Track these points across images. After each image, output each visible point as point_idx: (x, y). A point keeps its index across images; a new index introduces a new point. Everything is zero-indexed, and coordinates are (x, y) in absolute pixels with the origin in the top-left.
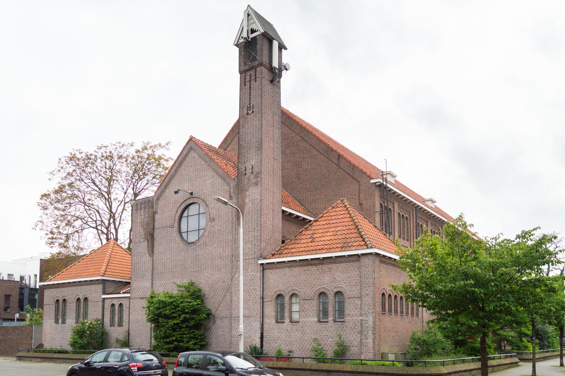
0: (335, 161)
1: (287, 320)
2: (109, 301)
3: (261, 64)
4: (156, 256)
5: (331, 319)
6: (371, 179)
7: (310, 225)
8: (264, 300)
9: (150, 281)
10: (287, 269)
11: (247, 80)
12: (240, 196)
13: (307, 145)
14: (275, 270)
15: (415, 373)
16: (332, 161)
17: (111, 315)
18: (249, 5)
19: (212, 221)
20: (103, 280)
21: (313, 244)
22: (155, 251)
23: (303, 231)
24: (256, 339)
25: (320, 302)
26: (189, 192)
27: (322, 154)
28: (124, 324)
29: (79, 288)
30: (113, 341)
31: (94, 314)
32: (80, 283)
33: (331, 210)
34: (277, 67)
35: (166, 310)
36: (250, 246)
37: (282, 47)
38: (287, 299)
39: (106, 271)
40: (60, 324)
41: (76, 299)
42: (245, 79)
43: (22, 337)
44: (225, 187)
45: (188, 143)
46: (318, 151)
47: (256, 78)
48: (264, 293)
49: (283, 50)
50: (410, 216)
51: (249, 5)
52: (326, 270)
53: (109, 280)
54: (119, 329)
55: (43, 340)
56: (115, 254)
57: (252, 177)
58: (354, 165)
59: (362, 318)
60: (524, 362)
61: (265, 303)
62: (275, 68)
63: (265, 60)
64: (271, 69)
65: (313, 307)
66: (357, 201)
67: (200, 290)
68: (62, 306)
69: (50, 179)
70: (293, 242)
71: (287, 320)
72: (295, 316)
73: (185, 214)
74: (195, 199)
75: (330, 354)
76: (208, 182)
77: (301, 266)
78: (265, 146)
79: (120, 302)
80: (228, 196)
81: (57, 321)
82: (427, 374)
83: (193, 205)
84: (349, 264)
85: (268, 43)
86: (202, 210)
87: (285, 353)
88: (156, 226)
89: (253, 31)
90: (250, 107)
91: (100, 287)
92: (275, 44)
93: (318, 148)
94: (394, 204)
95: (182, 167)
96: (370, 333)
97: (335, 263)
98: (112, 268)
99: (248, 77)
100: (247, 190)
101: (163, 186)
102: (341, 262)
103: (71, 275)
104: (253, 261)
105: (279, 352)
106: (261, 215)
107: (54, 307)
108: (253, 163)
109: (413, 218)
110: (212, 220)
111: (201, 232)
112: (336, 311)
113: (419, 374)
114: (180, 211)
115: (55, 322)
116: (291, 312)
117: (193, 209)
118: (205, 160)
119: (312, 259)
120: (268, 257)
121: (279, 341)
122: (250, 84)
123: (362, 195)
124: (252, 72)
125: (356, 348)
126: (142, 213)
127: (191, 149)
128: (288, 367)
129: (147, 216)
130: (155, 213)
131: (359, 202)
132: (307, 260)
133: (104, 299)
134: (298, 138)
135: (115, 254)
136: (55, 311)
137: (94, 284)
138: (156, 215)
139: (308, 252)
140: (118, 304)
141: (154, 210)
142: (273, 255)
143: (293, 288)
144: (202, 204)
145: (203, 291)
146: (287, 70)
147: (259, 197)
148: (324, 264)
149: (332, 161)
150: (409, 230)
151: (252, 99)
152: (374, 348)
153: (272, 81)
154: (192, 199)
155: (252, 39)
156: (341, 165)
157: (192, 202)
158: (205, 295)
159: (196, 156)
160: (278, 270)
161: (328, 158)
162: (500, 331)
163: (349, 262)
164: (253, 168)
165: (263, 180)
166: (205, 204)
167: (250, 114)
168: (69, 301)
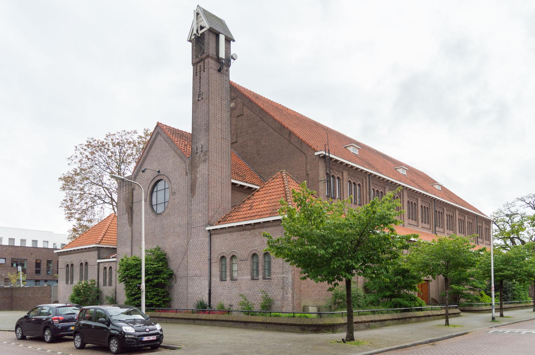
0: (287, 136)
1: (228, 278)
2: (103, 264)
3: (208, 56)
4: (134, 225)
5: (261, 276)
6: (315, 152)
7: (252, 195)
8: (212, 262)
9: (130, 247)
10: (228, 234)
11: (198, 71)
12: (193, 172)
13: (265, 125)
14: (219, 235)
15: (310, 323)
16: (284, 138)
17: (104, 277)
18: (198, 5)
19: (174, 194)
20: (97, 247)
21: (251, 211)
22: (134, 222)
23: (245, 200)
24: (205, 295)
25: (253, 262)
26: (157, 170)
27: (277, 132)
28: (113, 283)
29: (81, 254)
30: (104, 298)
31: (92, 275)
32: (82, 251)
33: (271, 181)
34: (224, 58)
35: (132, 271)
36: (201, 215)
37: (229, 40)
38: (228, 260)
39: (102, 239)
40: (69, 284)
41: (80, 264)
42: (196, 70)
43: (44, 296)
44: (183, 165)
45: (155, 129)
46: (273, 129)
47: (204, 68)
48: (212, 255)
49: (232, 42)
50: (363, 183)
51: (198, 5)
52: (257, 234)
53: (103, 247)
54: (110, 288)
55: (58, 298)
56: (113, 225)
57: (202, 154)
58: (302, 140)
59: (283, 275)
60: (473, 313)
61: (212, 264)
62: (221, 59)
63: (212, 51)
64: (218, 59)
65: (247, 266)
66: (304, 172)
67: (165, 255)
68: (71, 270)
69: (69, 164)
70: (236, 210)
71: (228, 278)
72: (235, 275)
73: (155, 190)
74: (161, 176)
75: (257, 307)
76: (171, 161)
77: (238, 231)
78: (213, 127)
79: (110, 266)
80: (185, 172)
81: (67, 283)
82: (321, 324)
83: (160, 182)
84: (274, 228)
85: (215, 37)
86: (167, 186)
87: (227, 307)
88: (134, 201)
89: (202, 28)
90: (200, 95)
91: (95, 253)
92: (222, 38)
93: (273, 126)
94: (343, 173)
95: (152, 149)
96: (290, 289)
97: (263, 227)
98: (109, 237)
99: (198, 68)
100: (197, 167)
101: (139, 166)
102: (268, 227)
103: (78, 244)
104: (202, 228)
105: (222, 307)
106: (208, 188)
107: (65, 271)
108: (202, 143)
109: (366, 185)
110: (173, 193)
111: (166, 204)
112: (265, 269)
113: (313, 324)
114: (151, 187)
115: (66, 283)
116: (232, 271)
117: (161, 185)
118: (168, 142)
119: (246, 225)
120: (215, 224)
121: (222, 297)
122: (200, 74)
123: (308, 166)
124: (202, 64)
125: (280, 302)
126: (124, 190)
127: (158, 133)
128: (216, 319)
129: (127, 192)
130: (133, 189)
131: (306, 172)
132: (242, 225)
133: (99, 263)
134: (258, 118)
135: (113, 225)
136: (66, 274)
137: (91, 251)
138: (134, 191)
139: (245, 219)
140: (109, 267)
141: (133, 187)
142: (219, 222)
143: (232, 251)
144: (167, 180)
145: (168, 255)
146: (234, 59)
147: (207, 172)
148: (255, 229)
149: (284, 138)
150: (362, 196)
151: (201, 87)
152: (293, 302)
153: (219, 71)
154: (159, 176)
155: (201, 34)
156: (292, 140)
157: (159, 179)
158: (169, 258)
159: (162, 139)
160: (221, 235)
161: (281, 135)
162: (452, 285)
163: (274, 226)
164: (202, 147)
165: (210, 157)
166: (168, 180)
167: (200, 100)
168: (75, 266)
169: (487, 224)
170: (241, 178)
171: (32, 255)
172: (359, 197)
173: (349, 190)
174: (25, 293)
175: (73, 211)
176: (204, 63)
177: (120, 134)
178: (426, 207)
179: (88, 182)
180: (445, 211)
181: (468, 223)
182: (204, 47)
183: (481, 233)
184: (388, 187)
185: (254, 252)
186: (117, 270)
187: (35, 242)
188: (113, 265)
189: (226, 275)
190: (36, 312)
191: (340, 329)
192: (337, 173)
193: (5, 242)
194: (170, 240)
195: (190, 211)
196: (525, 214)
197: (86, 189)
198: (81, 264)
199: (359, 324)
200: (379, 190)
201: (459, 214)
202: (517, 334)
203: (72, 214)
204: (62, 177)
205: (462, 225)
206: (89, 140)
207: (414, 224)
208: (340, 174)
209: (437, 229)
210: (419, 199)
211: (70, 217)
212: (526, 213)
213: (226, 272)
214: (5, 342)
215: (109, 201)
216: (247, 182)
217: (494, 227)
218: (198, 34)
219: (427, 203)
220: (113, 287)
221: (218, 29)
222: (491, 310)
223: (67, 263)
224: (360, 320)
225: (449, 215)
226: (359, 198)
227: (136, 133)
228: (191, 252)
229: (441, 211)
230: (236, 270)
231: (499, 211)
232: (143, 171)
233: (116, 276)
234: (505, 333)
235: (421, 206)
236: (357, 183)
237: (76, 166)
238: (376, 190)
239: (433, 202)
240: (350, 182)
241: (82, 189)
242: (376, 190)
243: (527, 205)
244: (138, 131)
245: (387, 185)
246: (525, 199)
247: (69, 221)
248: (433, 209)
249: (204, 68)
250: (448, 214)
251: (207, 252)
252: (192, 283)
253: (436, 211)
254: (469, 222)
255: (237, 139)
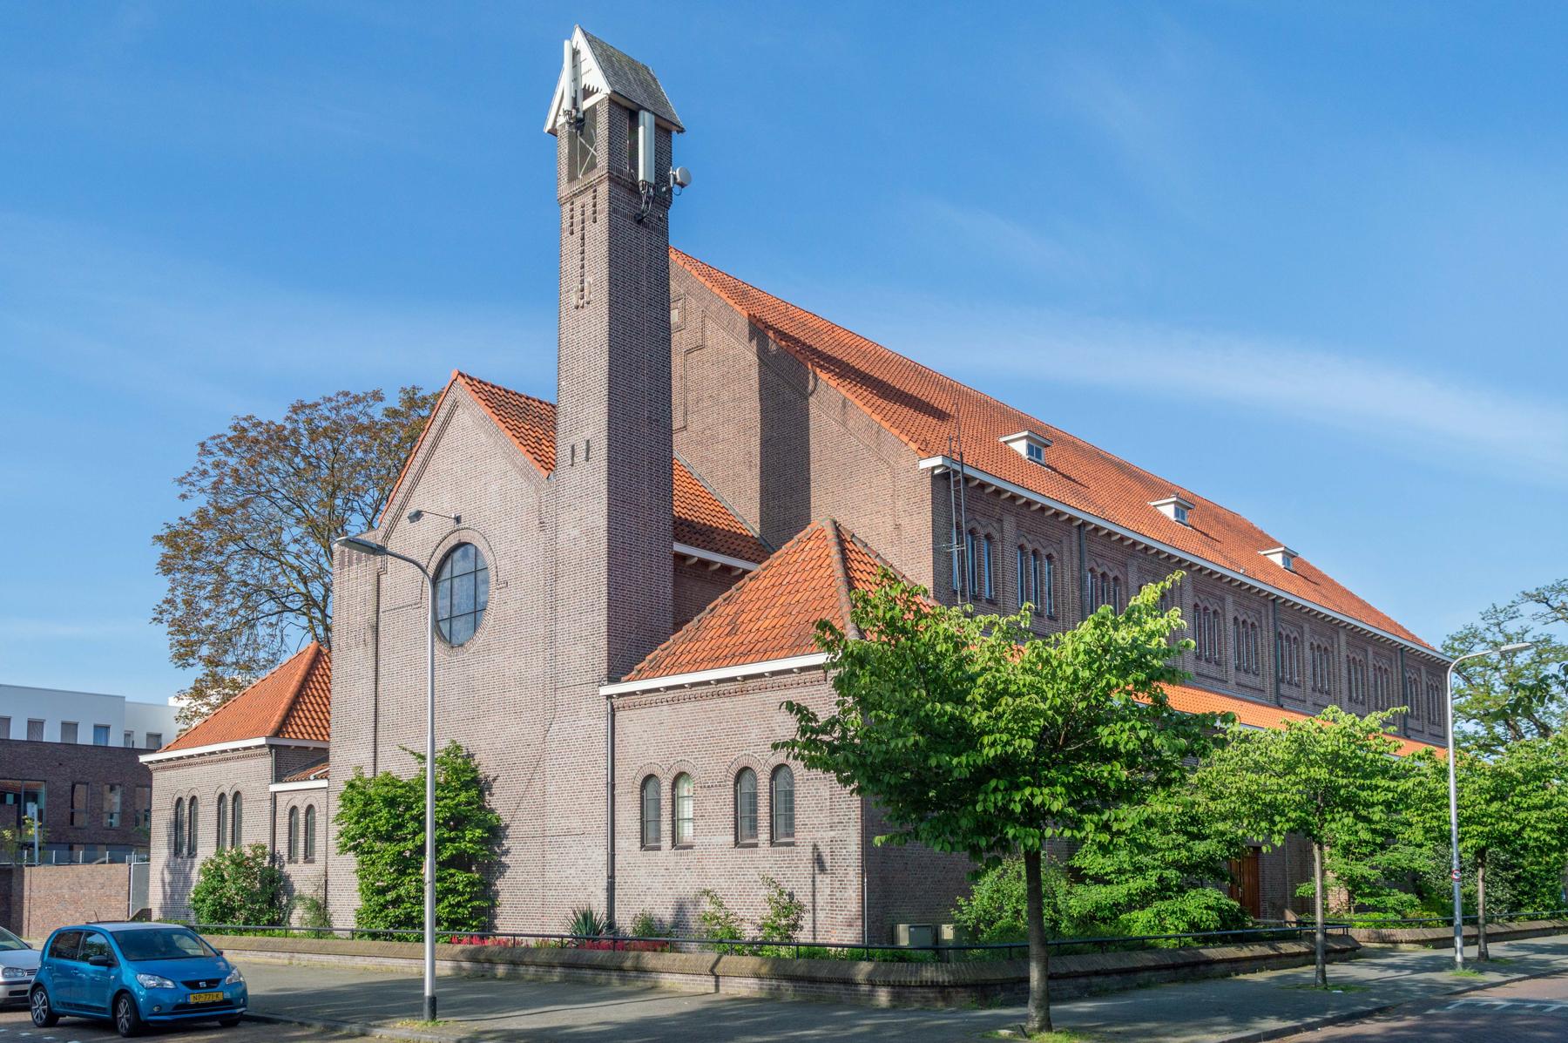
1: (666, 842)
11: (575, 220)
28: (317, 857)
31: (254, 833)
36: (583, 652)
42: (572, 218)
59: (832, 834)
61: (617, 799)
65: (722, 805)
71: (666, 842)
72: (686, 832)
76: (494, 487)
80: (537, 522)
89: (588, 93)
104: (588, 689)
121: (649, 898)
122: (583, 229)
124: (590, 194)
139: (716, 661)
156: (851, 424)
169: (1433, 675)
170: (701, 538)
171: (62, 768)
172: (1050, 594)
173: (1022, 573)
174: (51, 884)
175: (194, 637)
176: (595, 197)
177: (334, 404)
178: (1249, 621)
179: (238, 549)
180: (1307, 636)
181: (1349, 661)
182: (595, 150)
183: (1417, 701)
184: (1136, 563)
185: (744, 763)
186: (333, 815)
187: (70, 728)
188: (318, 801)
189: (658, 830)
190: (1275, 950)
191: (1002, 996)
192: (984, 521)
193: (18, 732)
194: (490, 726)
195: (551, 639)
196: (1548, 641)
197: (232, 568)
198: (222, 797)
199: (1061, 982)
200: (1108, 572)
201: (1348, 643)
202: (1531, 1011)
203: (193, 644)
204: (165, 532)
205: (1359, 676)
206: (243, 424)
207: (1214, 675)
208: (995, 525)
209: (1284, 689)
210: (1229, 599)
211: (184, 655)
212: (1553, 640)
213: (658, 822)
214: (24, 1034)
215: (300, 604)
216: (717, 551)
217: (1453, 680)
218: (578, 110)
219: (1252, 610)
220: (318, 866)
221: (639, 96)
222: (1452, 939)
223: (179, 795)
224: (1063, 970)
225: (1319, 646)
226: (1050, 598)
227: (381, 399)
228: (554, 762)
229: (1295, 634)
230: (691, 816)
231: (1467, 632)
232: (417, 515)
233: (328, 834)
234: (1547, 1010)
235: (1236, 619)
236: (1044, 552)
237: (200, 501)
238: (1099, 571)
239: (1399, 655)
240: (1021, 547)
241: (219, 570)
242: (1099, 571)
243: (1553, 615)
244: (386, 393)
245: (1133, 556)
246: (1547, 595)
247: (184, 666)
248: (1271, 628)
249: (595, 212)
250: (1315, 644)
251: (603, 763)
252: (556, 856)
253: (1280, 633)
254: (1380, 667)
255: (685, 420)
